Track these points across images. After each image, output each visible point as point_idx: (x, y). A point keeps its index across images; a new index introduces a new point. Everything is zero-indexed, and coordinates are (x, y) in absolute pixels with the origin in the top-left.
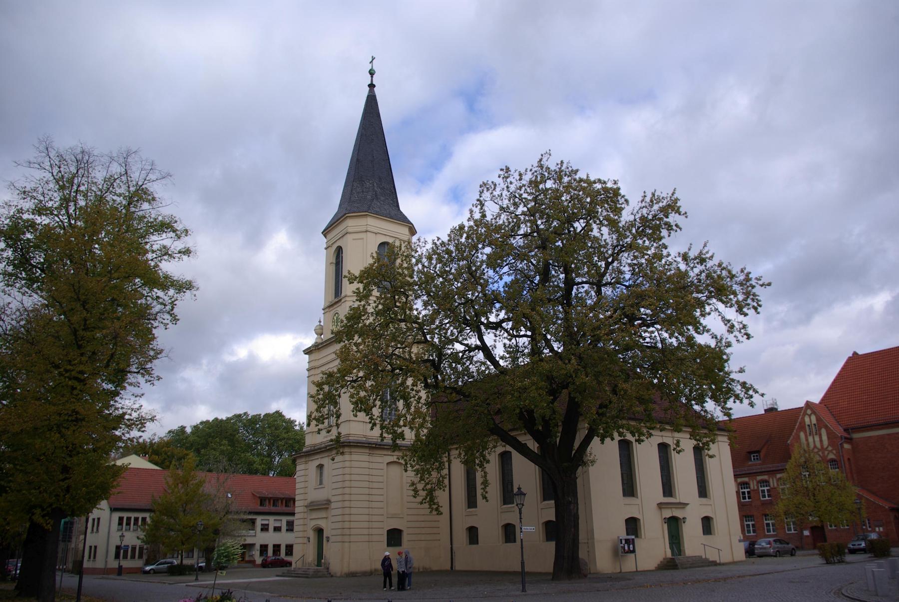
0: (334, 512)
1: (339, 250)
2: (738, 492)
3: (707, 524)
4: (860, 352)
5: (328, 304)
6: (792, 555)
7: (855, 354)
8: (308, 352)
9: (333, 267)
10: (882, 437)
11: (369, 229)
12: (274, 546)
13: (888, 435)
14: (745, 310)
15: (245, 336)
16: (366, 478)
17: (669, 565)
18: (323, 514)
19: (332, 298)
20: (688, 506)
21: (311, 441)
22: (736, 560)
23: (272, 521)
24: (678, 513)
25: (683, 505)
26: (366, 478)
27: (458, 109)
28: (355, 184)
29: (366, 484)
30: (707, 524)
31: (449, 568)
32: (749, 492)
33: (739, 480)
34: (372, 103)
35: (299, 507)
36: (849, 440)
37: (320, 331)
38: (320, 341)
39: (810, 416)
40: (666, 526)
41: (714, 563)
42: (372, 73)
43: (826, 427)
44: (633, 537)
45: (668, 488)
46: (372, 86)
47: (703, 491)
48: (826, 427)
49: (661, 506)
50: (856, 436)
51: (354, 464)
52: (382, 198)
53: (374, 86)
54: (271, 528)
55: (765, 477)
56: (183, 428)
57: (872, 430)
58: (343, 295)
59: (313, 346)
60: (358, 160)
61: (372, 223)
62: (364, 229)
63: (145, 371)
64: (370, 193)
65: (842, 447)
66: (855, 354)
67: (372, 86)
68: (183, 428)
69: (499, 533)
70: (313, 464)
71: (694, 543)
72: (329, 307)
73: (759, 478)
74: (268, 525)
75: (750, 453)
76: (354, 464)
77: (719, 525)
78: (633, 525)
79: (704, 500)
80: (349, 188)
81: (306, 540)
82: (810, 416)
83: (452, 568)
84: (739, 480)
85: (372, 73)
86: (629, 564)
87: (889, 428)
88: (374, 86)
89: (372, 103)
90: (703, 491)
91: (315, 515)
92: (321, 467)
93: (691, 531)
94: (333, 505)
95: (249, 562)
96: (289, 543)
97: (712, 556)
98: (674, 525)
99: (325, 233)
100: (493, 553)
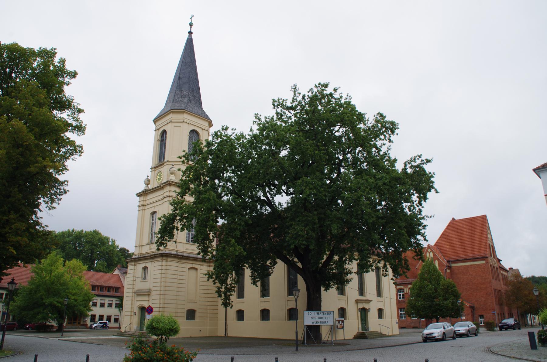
0: (154, 297)
1: (164, 133)
2: (397, 294)
3: (380, 311)
4: (456, 219)
5: (154, 166)
6: (476, 335)
7: (453, 219)
8: (139, 195)
9: (159, 143)
10: (467, 266)
11: (185, 121)
12: (100, 316)
13: (471, 265)
15: (108, 178)
16: (176, 277)
17: (361, 336)
18: (146, 298)
19: (157, 162)
20: (371, 303)
21: (67, 262)
22: (394, 334)
23: (107, 301)
24: (366, 306)
25: (368, 301)
26: (176, 277)
28: (177, 92)
29: (176, 281)
30: (380, 311)
31: (224, 335)
32: (403, 295)
33: (398, 287)
34: (190, 44)
35: (127, 295)
36: (450, 268)
37: (148, 182)
38: (147, 188)
39: (429, 253)
40: (359, 313)
41: (385, 336)
42: (191, 25)
43: (438, 260)
44: (343, 319)
45: (362, 291)
46: (190, 33)
47: (379, 293)
48: (438, 260)
49: (357, 301)
50: (453, 265)
51: (168, 267)
52: (194, 102)
53: (192, 33)
54: (106, 305)
55: (402, 287)
56: (82, 231)
57: (462, 262)
58: (165, 160)
59: (143, 192)
60: (179, 77)
61: (186, 117)
62: (182, 120)
64: (187, 99)
65: (446, 271)
66: (453, 219)
67: (190, 33)
68: (82, 231)
69: (258, 314)
70: (140, 266)
71: (374, 323)
72: (154, 168)
74: (96, 303)
76: (168, 267)
77: (387, 313)
78: (343, 312)
79: (341, 296)
80: (173, 94)
81: (133, 314)
82: (429, 253)
83: (225, 334)
84: (398, 287)
85: (191, 25)
86: (340, 336)
87: (471, 261)
88: (192, 33)
89: (190, 44)
90: (379, 293)
91: (140, 298)
92: (145, 268)
93: (373, 316)
94: (153, 293)
95: (83, 325)
96: (101, 314)
97: (384, 331)
98: (364, 312)
99: (155, 121)
100: (253, 327)
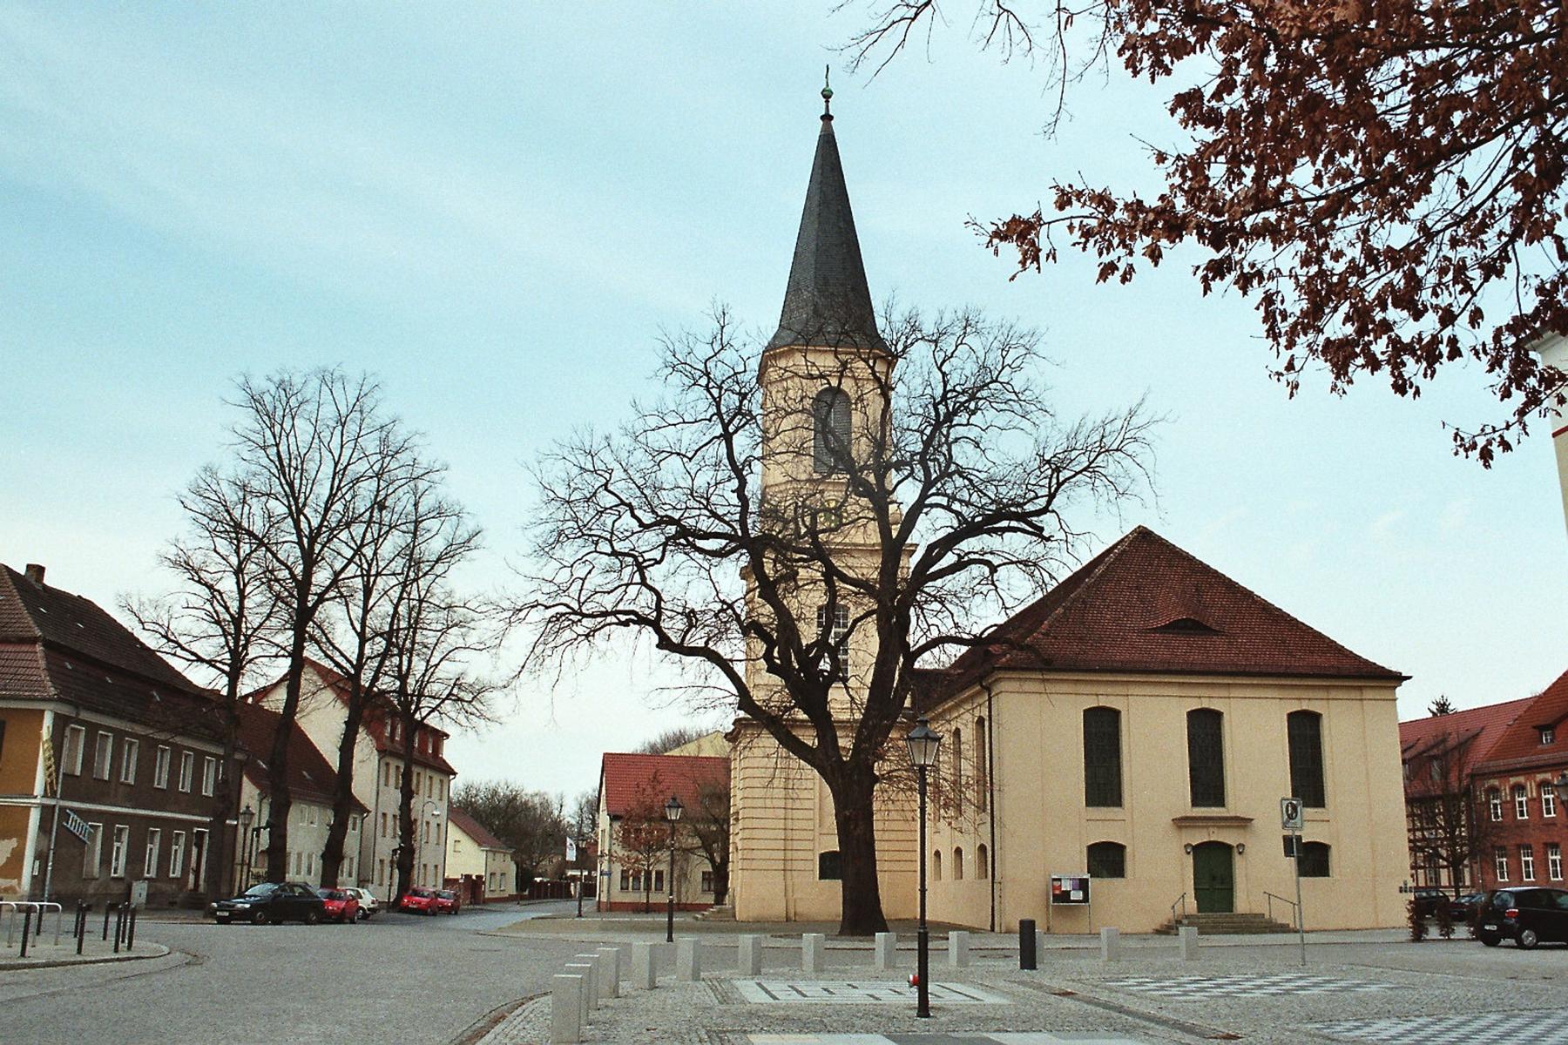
14: (1181, 111)
24: (1229, 837)
25: (1242, 823)
27: (1310, 833)
34: (828, 147)
42: (827, 95)
46: (827, 118)
49: (1182, 823)
53: (831, 118)
63: (515, 798)
67: (827, 118)
73: (1540, 777)
75: (1541, 729)
85: (827, 95)
88: (831, 118)
89: (828, 147)
